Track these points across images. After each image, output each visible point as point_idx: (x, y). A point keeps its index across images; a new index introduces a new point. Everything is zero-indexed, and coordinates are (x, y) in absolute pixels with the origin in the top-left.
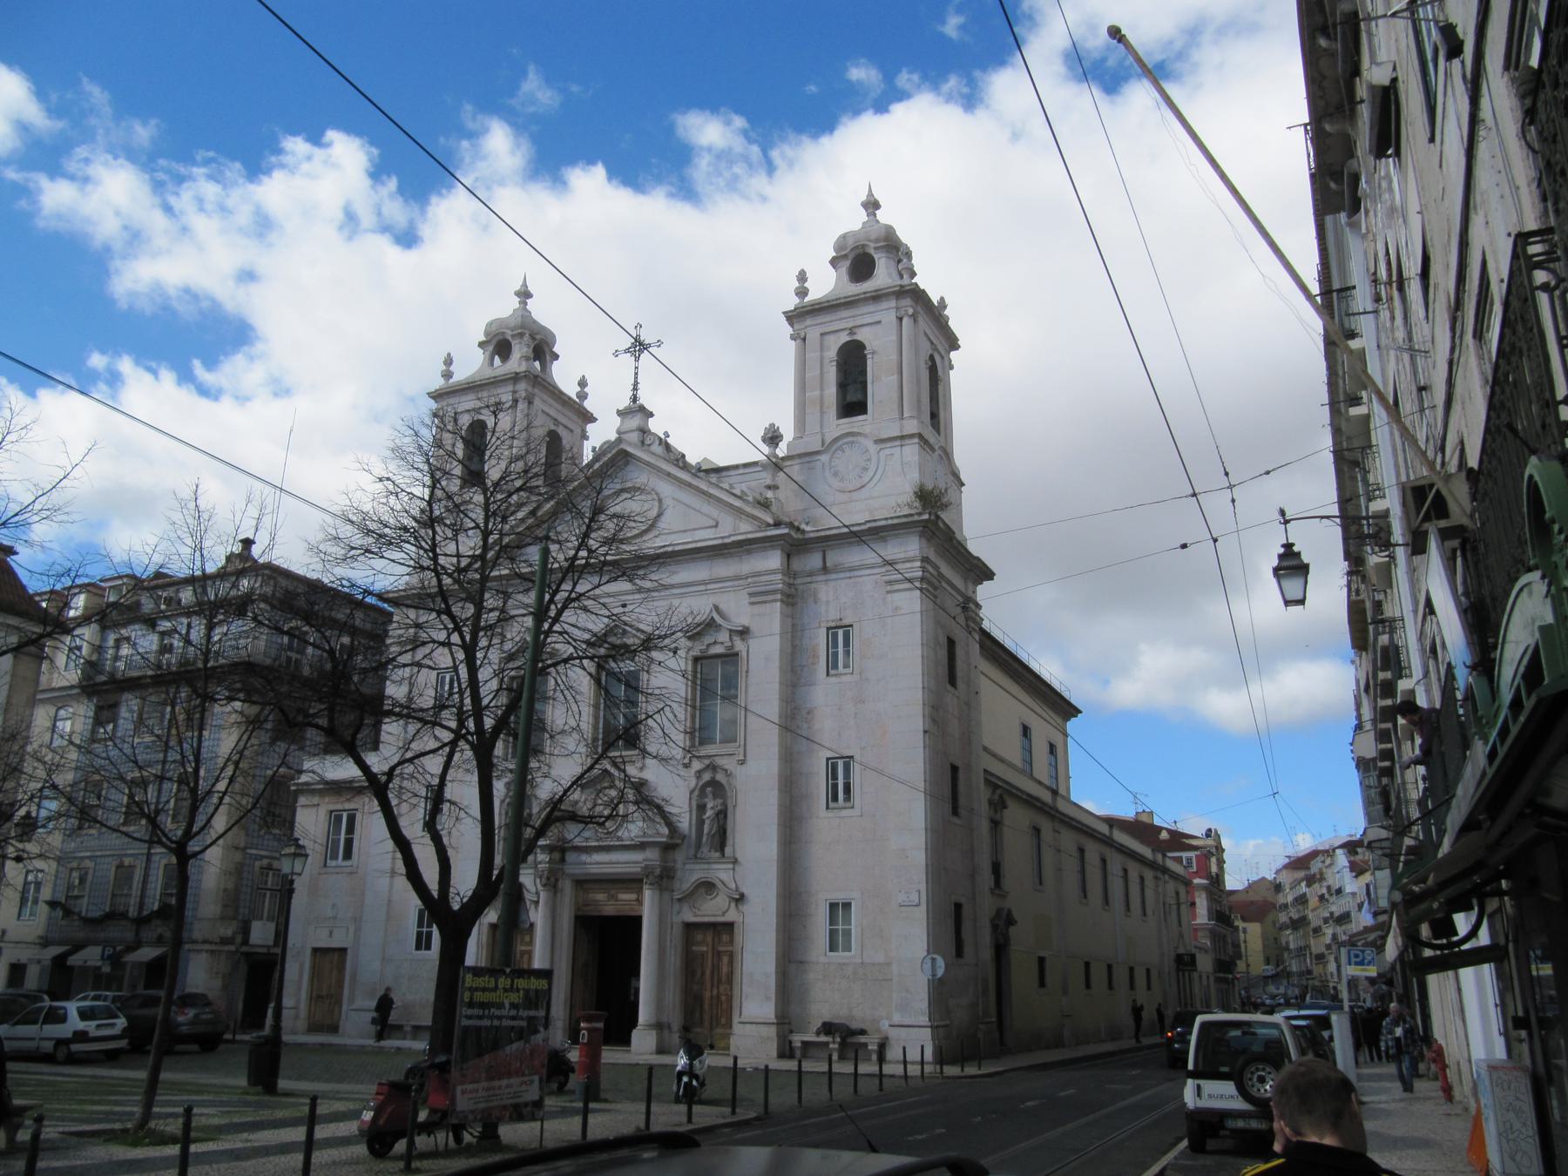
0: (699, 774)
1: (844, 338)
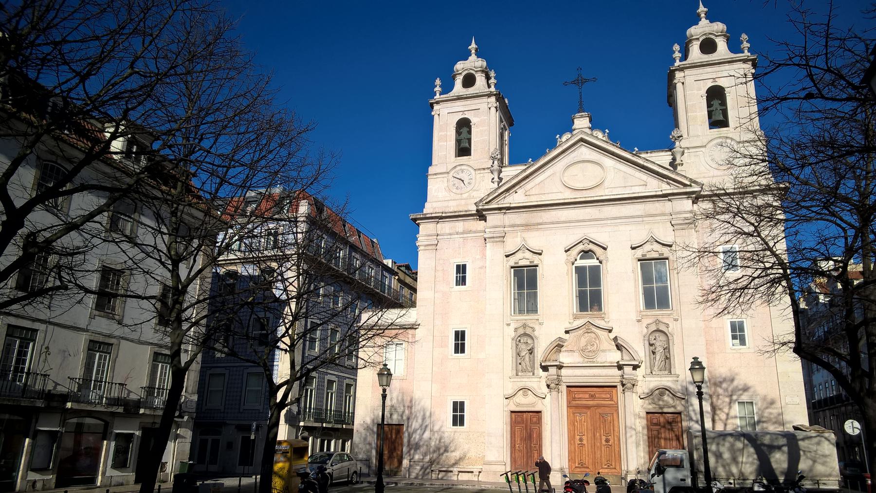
0: (516, 329)
1: (710, 84)
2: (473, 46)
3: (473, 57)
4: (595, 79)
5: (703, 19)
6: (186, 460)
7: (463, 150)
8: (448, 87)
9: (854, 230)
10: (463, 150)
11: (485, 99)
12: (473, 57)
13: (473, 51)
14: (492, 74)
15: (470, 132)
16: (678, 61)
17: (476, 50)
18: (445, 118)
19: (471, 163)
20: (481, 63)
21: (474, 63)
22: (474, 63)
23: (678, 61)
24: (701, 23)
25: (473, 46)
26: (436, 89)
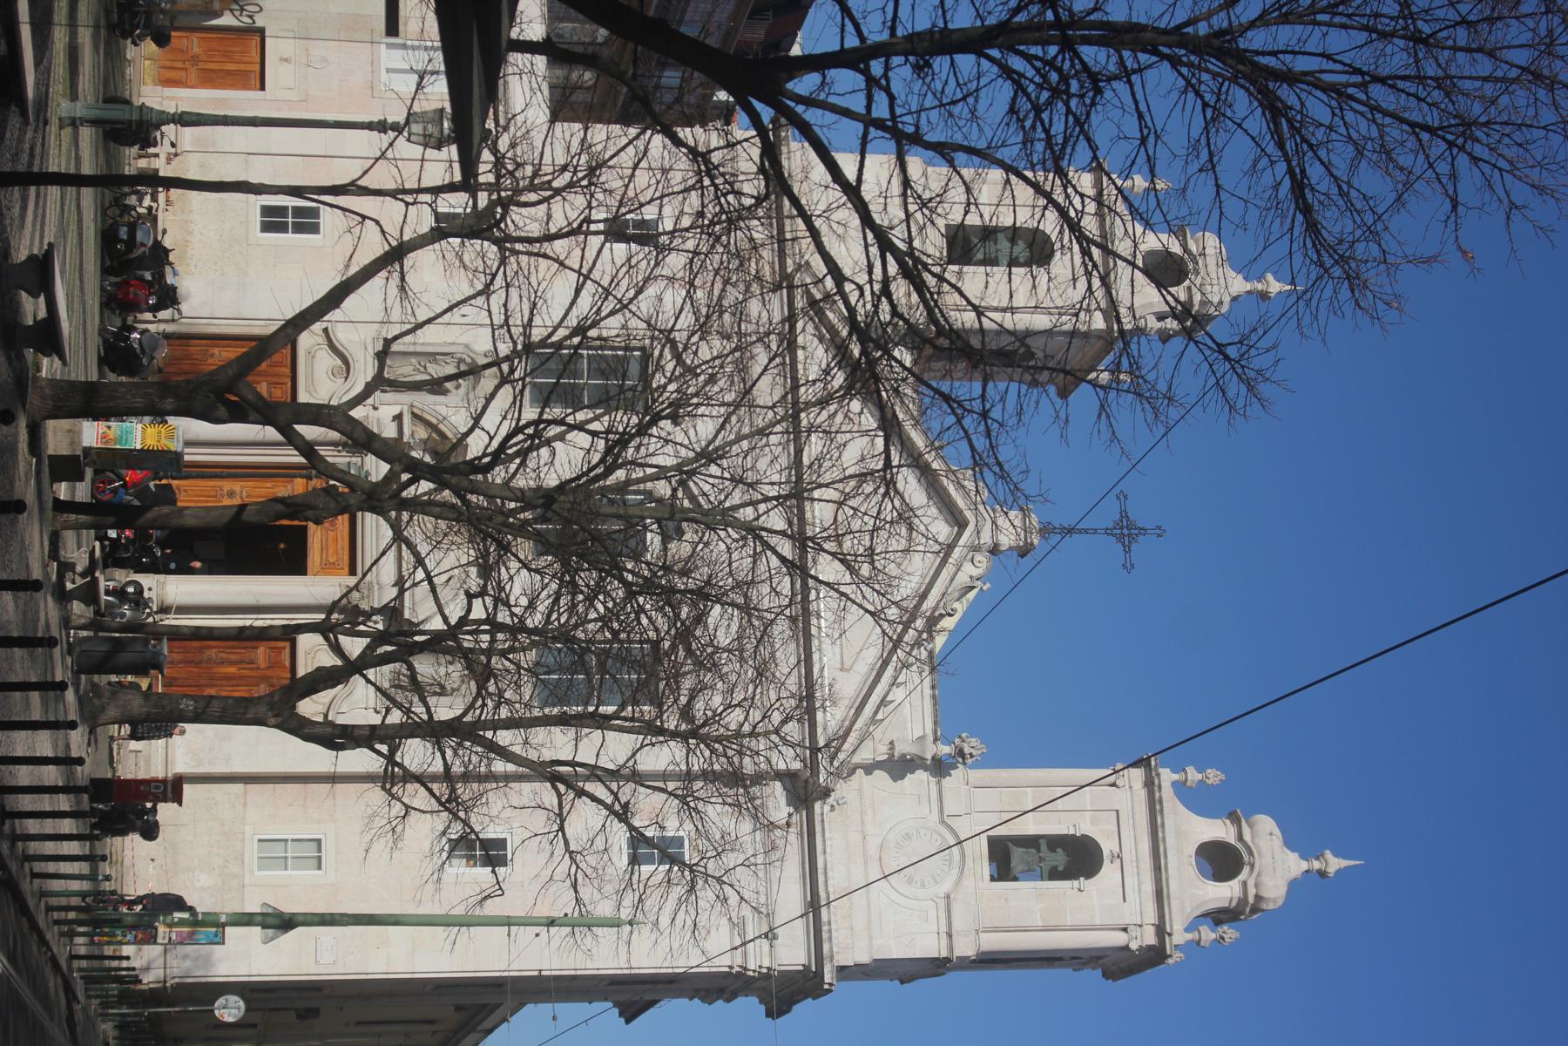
2: (1334, 864)
3: (1295, 865)
4: (1128, 567)
5: (1304, 866)
6: (311, 526)
7: (1005, 857)
8: (1198, 800)
9: (669, 492)
10: (1005, 857)
11: (1151, 917)
12: (1295, 865)
13: (1316, 865)
14: (1230, 933)
15: (1055, 875)
16: (1176, 777)
17: (1322, 874)
18: (1102, 806)
19: (968, 882)
20: (1275, 890)
21: (1276, 866)
22: (1276, 866)
23: (1176, 777)
24: (1293, 857)
25: (1334, 864)
26: (1190, 770)
